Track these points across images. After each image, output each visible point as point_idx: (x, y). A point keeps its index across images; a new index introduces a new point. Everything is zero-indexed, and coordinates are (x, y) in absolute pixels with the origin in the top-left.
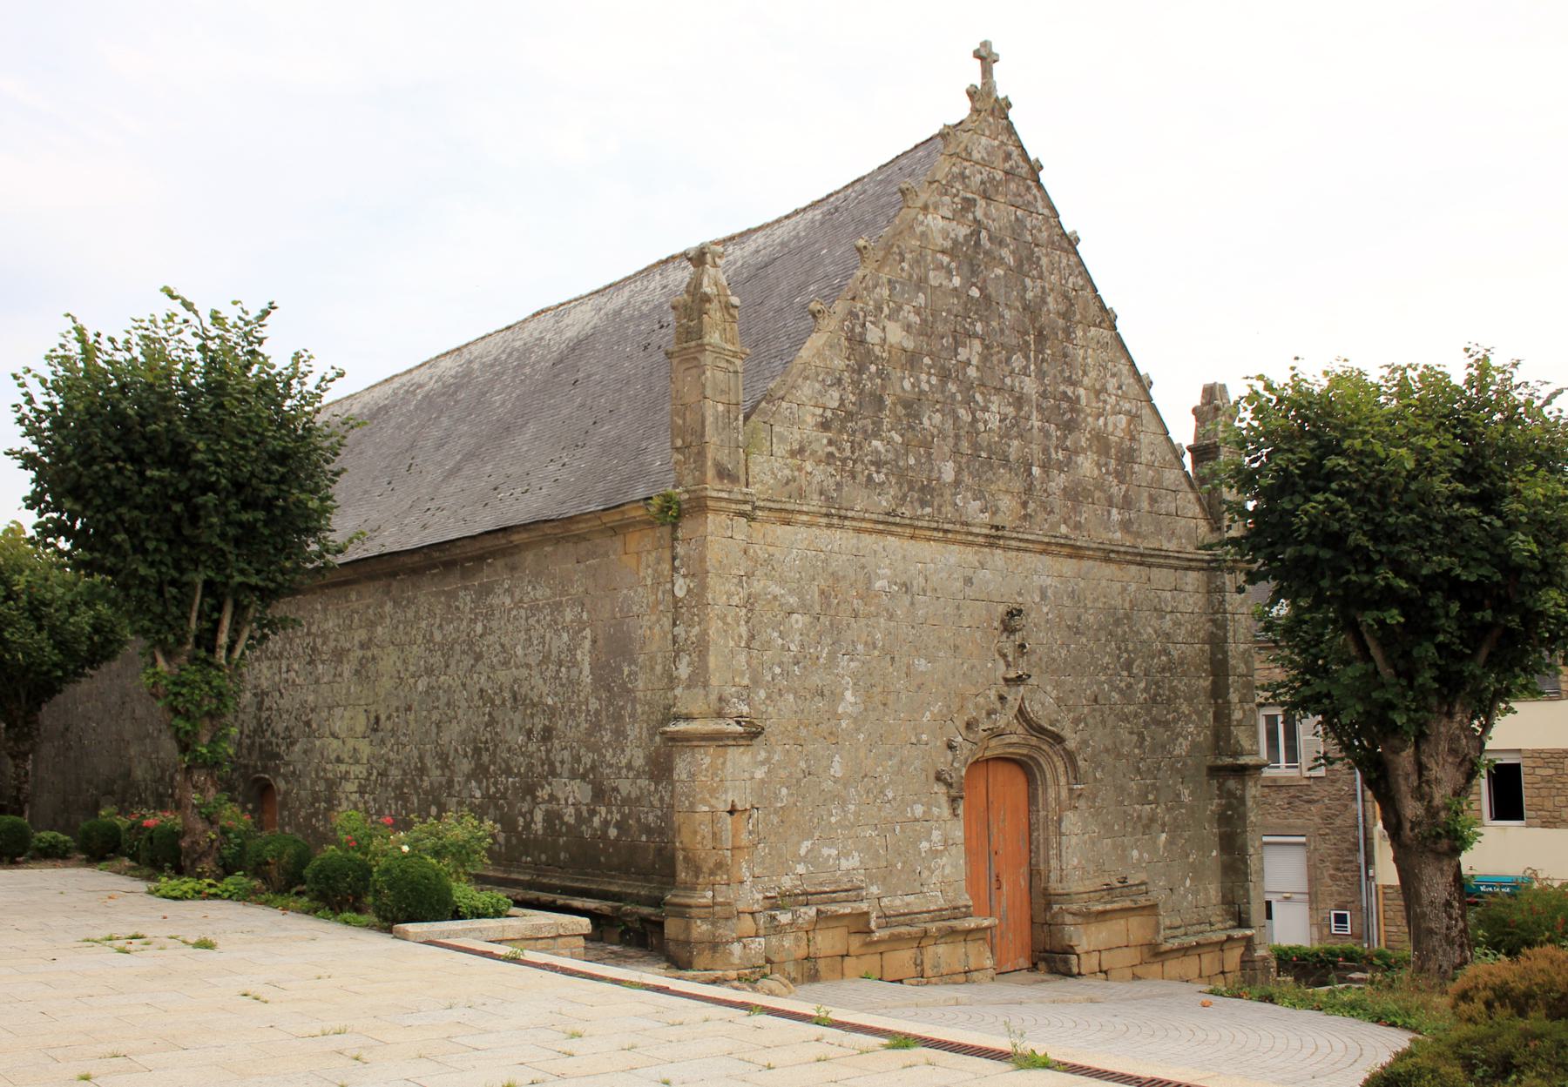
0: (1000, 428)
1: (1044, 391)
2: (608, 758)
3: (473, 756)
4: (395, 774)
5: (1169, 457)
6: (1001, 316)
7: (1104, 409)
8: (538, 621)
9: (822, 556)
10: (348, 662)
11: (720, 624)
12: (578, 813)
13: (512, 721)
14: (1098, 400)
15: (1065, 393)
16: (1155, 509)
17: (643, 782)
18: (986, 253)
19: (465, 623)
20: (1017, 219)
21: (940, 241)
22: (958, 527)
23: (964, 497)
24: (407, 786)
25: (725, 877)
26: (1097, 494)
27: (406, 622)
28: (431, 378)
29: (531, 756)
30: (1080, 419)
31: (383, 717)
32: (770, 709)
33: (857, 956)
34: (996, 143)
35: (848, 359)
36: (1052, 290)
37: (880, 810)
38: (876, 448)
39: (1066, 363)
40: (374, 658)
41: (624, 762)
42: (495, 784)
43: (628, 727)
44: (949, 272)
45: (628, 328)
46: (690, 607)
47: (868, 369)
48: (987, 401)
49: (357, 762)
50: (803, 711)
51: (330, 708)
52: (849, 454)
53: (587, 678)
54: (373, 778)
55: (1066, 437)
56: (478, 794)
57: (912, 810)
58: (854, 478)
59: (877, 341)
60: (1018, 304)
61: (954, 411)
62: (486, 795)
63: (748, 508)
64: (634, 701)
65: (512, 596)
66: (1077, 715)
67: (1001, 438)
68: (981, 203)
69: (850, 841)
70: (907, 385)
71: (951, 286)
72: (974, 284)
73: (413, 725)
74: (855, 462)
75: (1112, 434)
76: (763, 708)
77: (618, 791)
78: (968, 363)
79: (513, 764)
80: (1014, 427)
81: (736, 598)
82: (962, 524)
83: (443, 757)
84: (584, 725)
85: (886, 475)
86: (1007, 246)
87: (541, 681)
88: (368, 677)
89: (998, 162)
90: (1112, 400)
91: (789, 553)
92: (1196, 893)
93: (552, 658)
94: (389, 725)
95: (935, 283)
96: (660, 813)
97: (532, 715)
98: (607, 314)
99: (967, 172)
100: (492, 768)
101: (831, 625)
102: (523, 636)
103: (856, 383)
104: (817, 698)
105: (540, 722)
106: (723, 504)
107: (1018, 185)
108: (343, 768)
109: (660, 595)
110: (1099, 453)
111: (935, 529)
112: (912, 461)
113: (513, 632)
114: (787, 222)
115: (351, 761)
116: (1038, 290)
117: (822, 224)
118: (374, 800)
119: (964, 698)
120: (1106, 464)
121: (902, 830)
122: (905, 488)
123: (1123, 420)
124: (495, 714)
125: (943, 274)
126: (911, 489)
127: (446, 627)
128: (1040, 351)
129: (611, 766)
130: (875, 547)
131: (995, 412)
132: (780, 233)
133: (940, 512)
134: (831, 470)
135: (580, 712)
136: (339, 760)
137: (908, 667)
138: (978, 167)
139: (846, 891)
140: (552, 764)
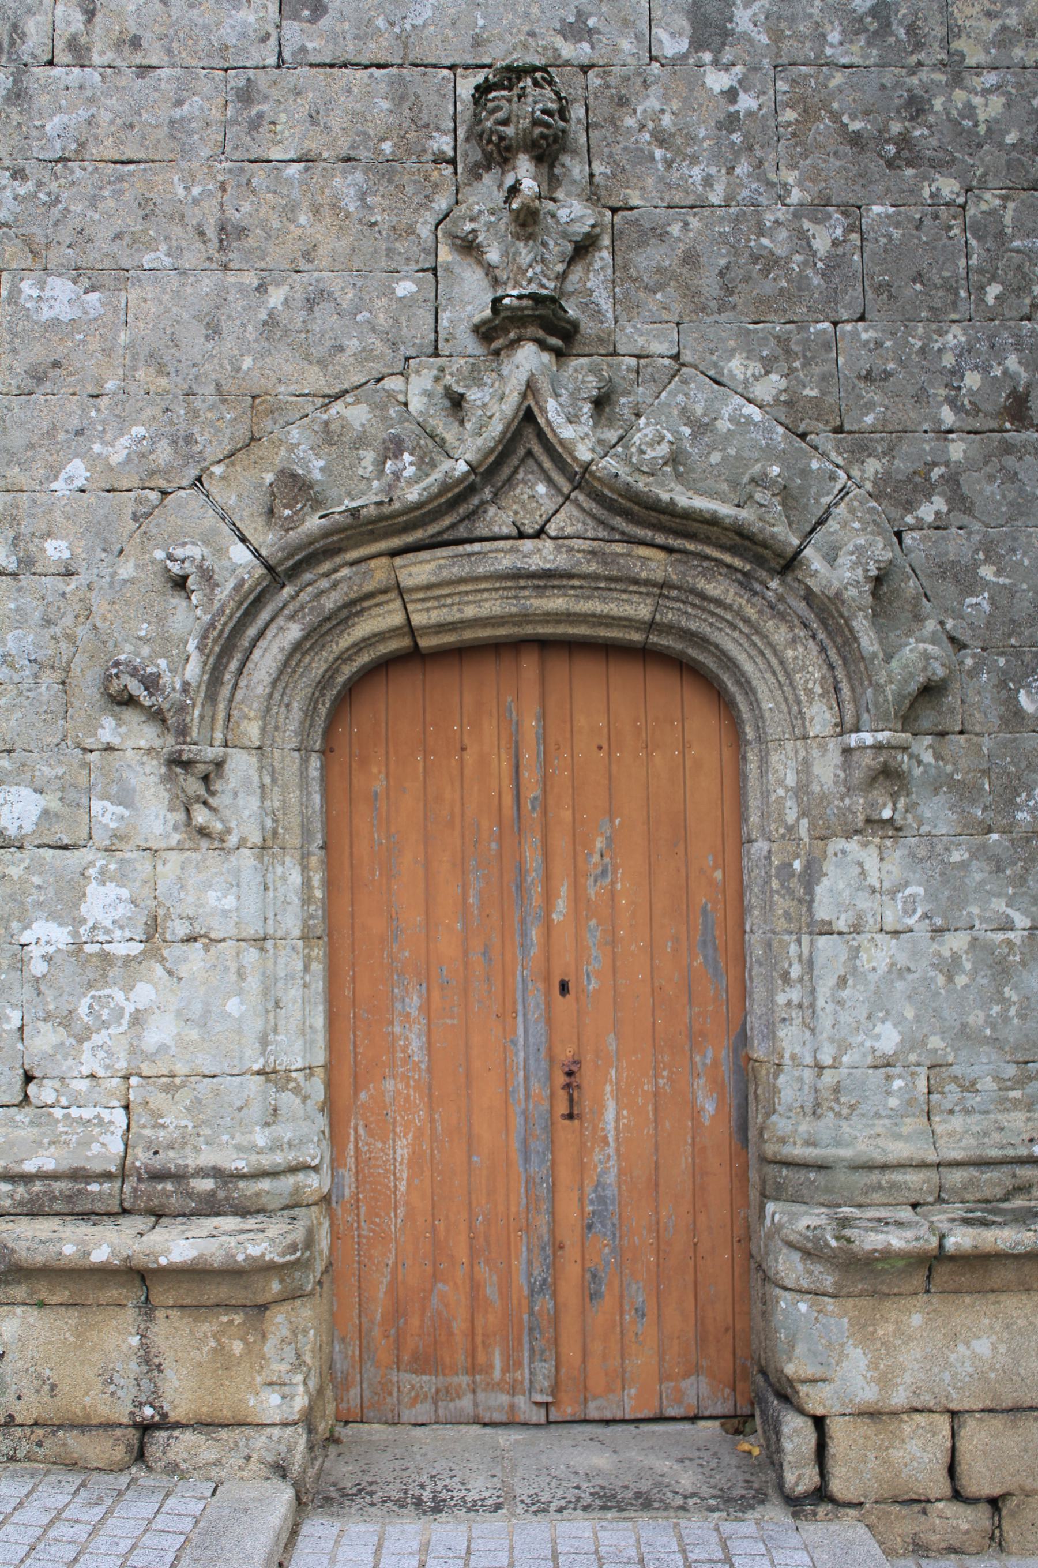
66: (902, 466)
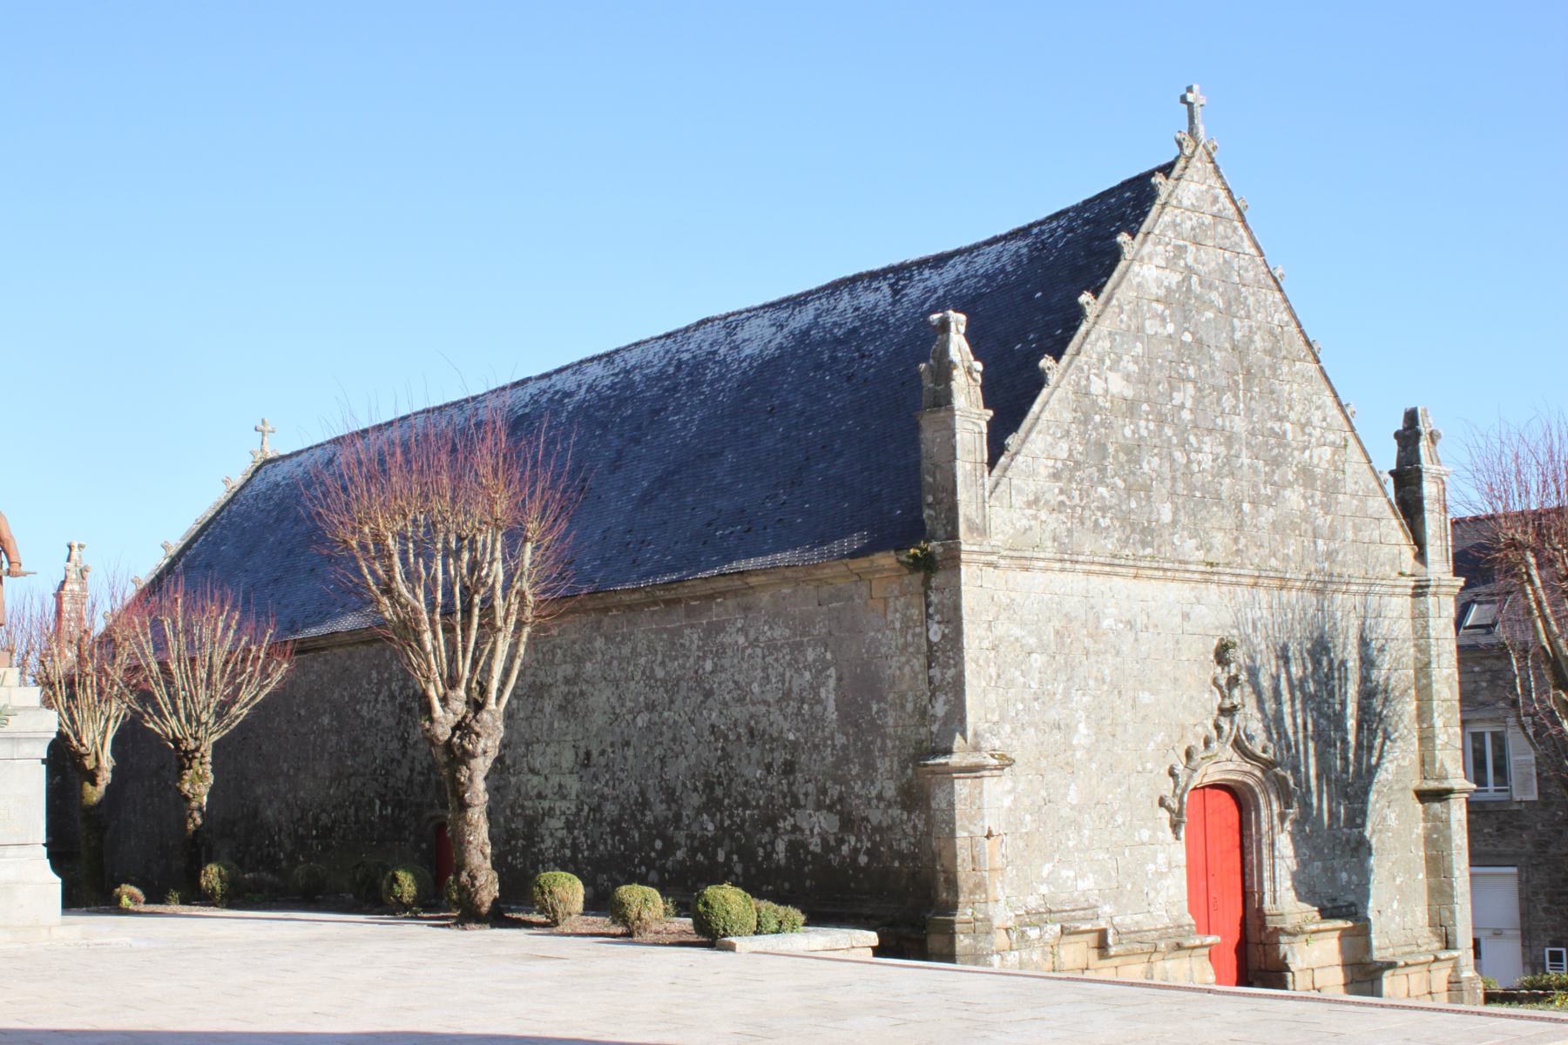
0: (1212, 467)
1: (1253, 428)
2: (856, 789)
3: (704, 791)
4: (610, 809)
5: (1374, 485)
6: (1212, 358)
7: (1310, 442)
8: (777, 660)
9: (1056, 599)
10: (551, 697)
11: (974, 665)
12: (824, 841)
13: (748, 756)
14: (1304, 433)
15: (1272, 429)
16: (1359, 537)
17: (896, 812)
18: (1197, 298)
19: (691, 660)
20: (1225, 261)
21: (1154, 290)
22: (1176, 566)
23: (1181, 537)
24: (626, 821)
25: (984, 896)
26: (1304, 526)
27: (621, 659)
28: (579, 386)
29: (771, 789)
30: (1287, 454)
31: (595, 753)
32: (1015, 742)
33: (1095, 970)
34: (1204, 187)
35: (1075, 411)
36: (1259, 328)
37: (1111, 834)
38: (1101, 494)
39: (1273, 400)
40: (582, 693)
41: (874, 793)
42: (731, 817)
43: (878, 761)
44: (1163, 319)
45: (822, 353)
46: (944, 652)
47: (1093, 419)
48: (1200, 442)
49: (564, 797)
50: (1042, 743)
51: (528, 745)
52: (1078, 502)
53: (832, 714)
54: (585, 812)
55: (1273, 471)
56: (711, 827)
57: (1139, 834)
58: (1083, 523)
59: (1100, 392)
60: (1227, 345)
61: (1170, 454)
62: (720, 827)
63: (994, 558)
64: (884, 736)
65: (747, 636)
67: (1214, 477)
68: (1192, 248)
69: (1085, 864)
70: (1128, 432)
71: (1166, 334)
72: (1187, 329)
73: (631, 761)
74: (1083, 508)
75: (1318, 466)
76: (1008, 741)
77: (868, 821)
78: (1182, 406)
79: (750, 797)
80: (1227, 466)
81: (986, 642)
82: (1180, 562)
83: (670, 796)
84: (830, 759)
85: (1111, 519)
86: (1217, 288)
87: (781, 718)
88: (574, 713)
89: (1206, 207)
90: (1317, 433)
91: (1029, 597)
92: (1403, 915)
93: (793, 695)
94: (603, 761)
95: (1150, 331)
96: (913, 840)
97: (772, 750)
98: (791, 333)
99: (1178, 220)
100: (726, 801)
101: (1066, 663)
102: (759, 674)
103: (1082, 434)
104: (1055, 731)
105: (780, 757)
106: (975, 556)
107: (1226, 227)
108: (546, 804)
109: (909, 638)
110: (1305, 486)
111: (1156, 569)
112: (1133, 505)
113: (748, 670)
114: (988, 249)
115: (556, 797)
116: (1246, 329)
117: (1031, 260)
118: (586, 835)
119: (1183, 728)
120: (1312, 497)
121: (1131, 855)
122: (1128, 530)
123: (1327, 452)
124: (729, 749)
125: (1157, 322)
126: (1133, 531)
127: (670, 664)
128: (1248, 390)
129: (858, 797)
130: (1103, 588)
131: (1207, 453)
132: (983, 263)
133: (1159, 552)
134: (1062, 517)
135: (825, 746)
136: (540, 796)
137: (1134, 700)
138: (1188, 213)
139: (1084, 909)
140: (795, 797)
